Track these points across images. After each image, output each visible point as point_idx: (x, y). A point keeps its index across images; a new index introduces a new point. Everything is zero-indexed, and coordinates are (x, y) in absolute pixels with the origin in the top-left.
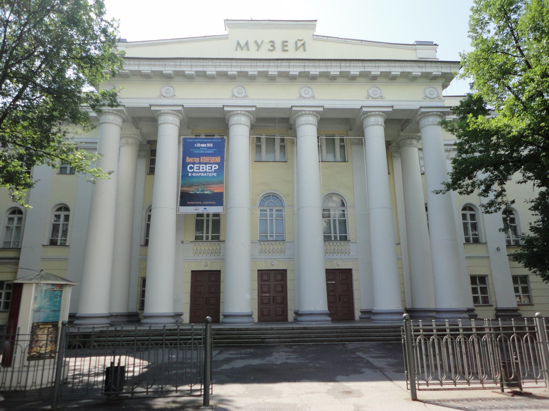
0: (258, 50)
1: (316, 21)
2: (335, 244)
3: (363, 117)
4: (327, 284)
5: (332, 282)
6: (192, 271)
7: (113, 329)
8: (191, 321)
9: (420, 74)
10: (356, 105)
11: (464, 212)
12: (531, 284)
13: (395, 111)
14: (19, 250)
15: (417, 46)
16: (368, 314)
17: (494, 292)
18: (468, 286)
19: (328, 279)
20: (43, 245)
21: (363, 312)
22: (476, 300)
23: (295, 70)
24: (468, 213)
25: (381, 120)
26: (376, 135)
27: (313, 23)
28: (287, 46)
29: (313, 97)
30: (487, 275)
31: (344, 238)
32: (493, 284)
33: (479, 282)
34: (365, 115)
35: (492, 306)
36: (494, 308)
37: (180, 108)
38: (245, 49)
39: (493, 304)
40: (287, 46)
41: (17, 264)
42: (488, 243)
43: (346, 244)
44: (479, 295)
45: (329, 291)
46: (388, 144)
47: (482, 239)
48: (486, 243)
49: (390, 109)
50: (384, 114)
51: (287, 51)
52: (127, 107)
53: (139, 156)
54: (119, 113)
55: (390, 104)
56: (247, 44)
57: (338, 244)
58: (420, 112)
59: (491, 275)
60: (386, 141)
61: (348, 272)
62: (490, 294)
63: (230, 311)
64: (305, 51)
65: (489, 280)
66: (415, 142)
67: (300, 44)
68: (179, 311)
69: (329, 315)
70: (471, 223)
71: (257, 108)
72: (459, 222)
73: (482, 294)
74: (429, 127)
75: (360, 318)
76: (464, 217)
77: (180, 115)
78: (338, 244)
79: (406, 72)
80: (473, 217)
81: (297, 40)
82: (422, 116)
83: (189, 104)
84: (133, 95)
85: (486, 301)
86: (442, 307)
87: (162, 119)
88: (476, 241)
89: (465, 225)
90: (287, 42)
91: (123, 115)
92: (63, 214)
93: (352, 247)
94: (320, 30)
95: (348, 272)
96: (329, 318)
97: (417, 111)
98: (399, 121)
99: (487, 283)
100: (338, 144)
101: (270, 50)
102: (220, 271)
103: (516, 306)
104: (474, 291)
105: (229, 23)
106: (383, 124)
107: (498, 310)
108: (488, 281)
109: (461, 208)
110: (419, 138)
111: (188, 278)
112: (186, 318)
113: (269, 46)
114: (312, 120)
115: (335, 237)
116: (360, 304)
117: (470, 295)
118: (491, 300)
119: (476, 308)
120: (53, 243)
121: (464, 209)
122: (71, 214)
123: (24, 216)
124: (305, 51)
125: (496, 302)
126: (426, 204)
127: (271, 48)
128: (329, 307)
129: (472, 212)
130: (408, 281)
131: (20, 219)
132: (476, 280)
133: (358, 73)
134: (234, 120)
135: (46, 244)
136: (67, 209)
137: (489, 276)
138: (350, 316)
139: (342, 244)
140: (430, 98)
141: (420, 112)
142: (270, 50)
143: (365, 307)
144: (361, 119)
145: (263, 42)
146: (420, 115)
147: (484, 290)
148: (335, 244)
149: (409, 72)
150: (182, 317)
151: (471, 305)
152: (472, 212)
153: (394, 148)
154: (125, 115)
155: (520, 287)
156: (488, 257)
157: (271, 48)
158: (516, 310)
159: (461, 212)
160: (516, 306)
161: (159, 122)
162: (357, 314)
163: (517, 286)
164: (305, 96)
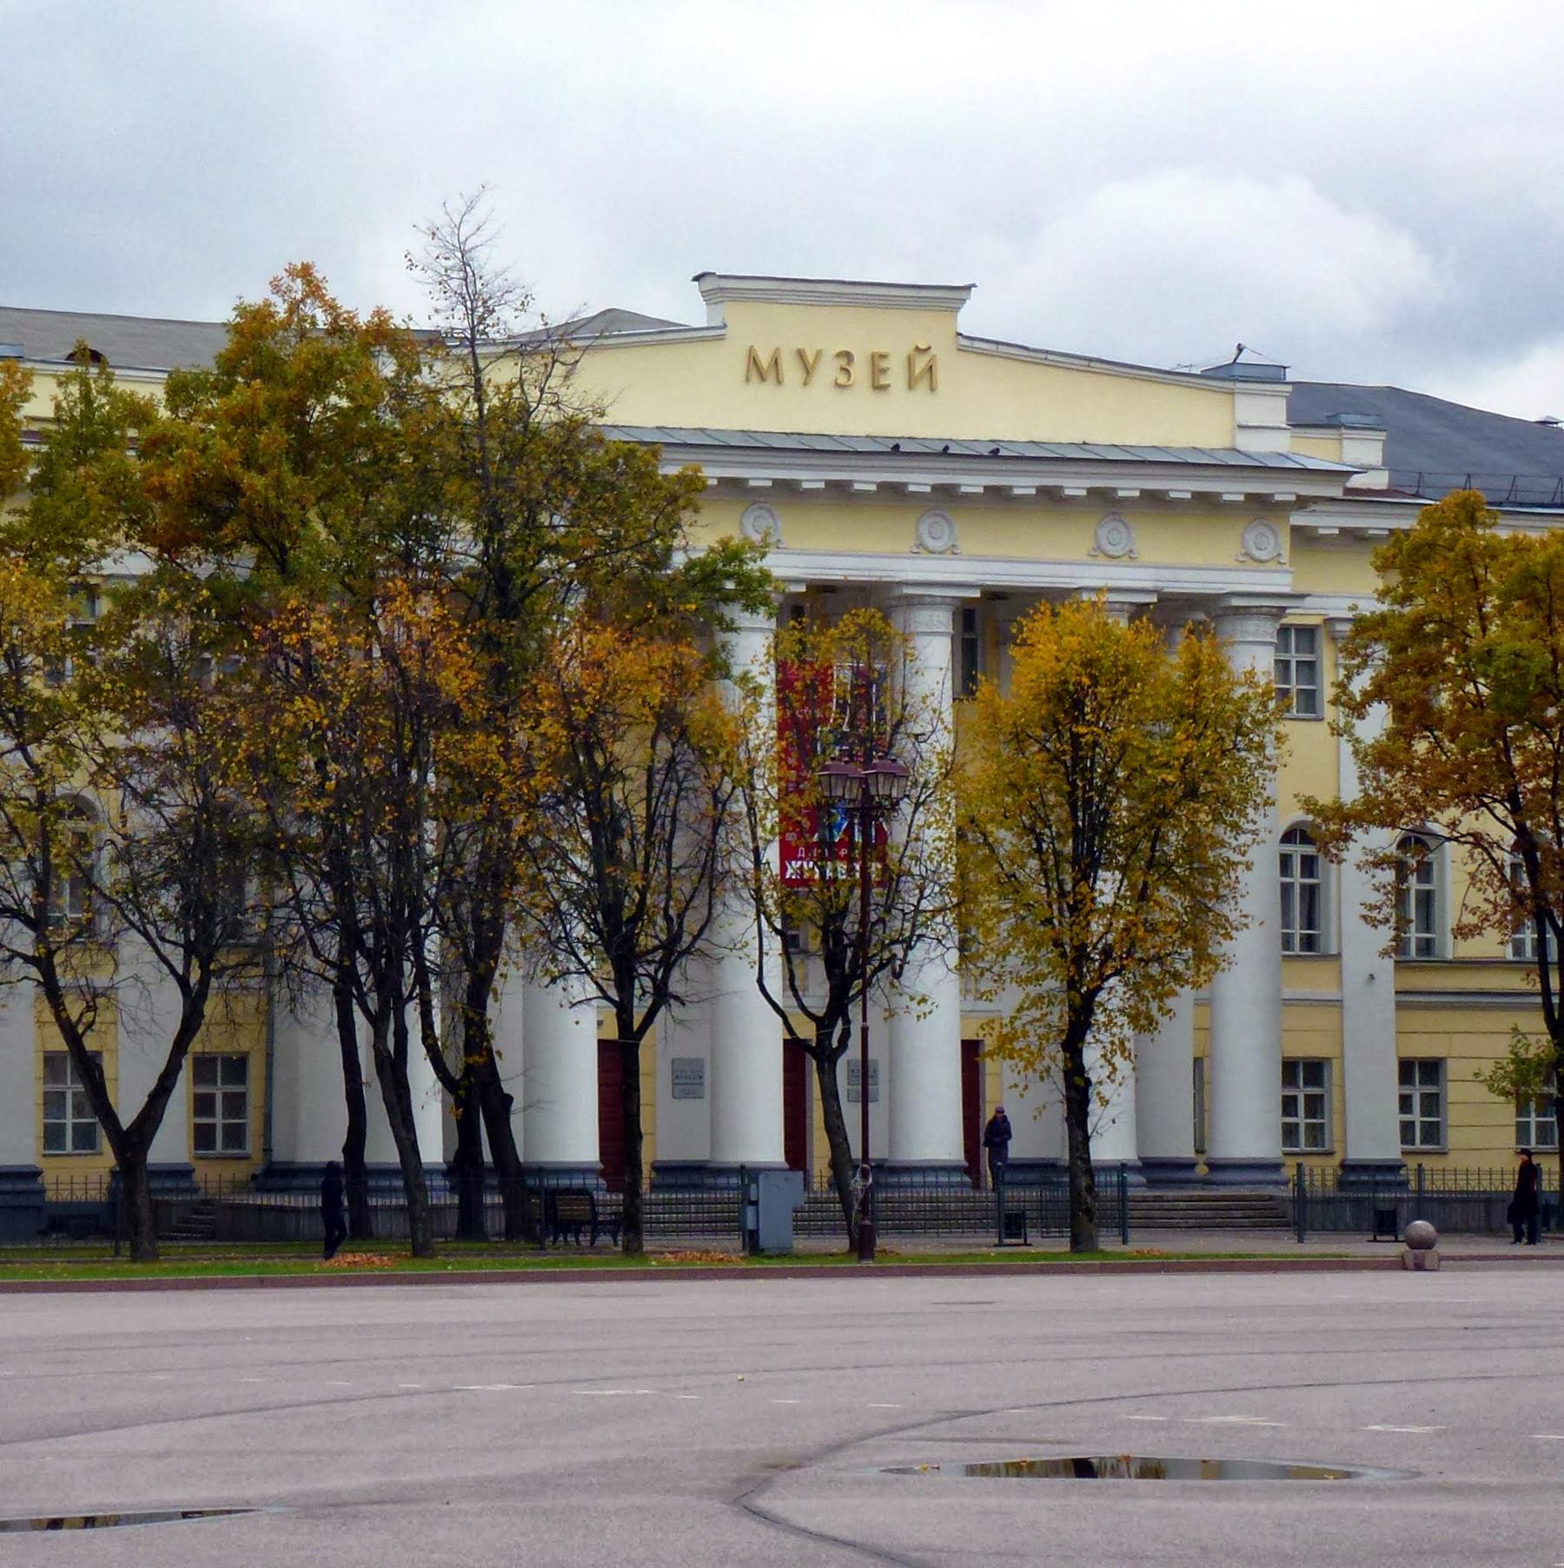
0: (805, 384)
7: (145, 1214)
11: (1288, 848)
17: (1344, 1112)
22: (1289, 1133)
24: (1298, 850)
28: (884, 371)
29: (953, 551)
30: (1328, 1059)
32: (1343, 1086)
35: (1330, 1154)
36: (1336, 1160)
38: (771, 378)
39: (1337, 1147)
40: (884, 371)
41: (1342, 1007)
42: (1345, 956)
44: (1301, 1119)
48: (1339, 955)
51: (884, 388)
56: (776, 362)
59: (1342, 1057)
62: (1331, 1120)
63: (544, 1159)
64: (932, 389)
65: (1333, 1074)
67: (921, 364)
74: (1245, 647)
81: (910, 349)
84: (799, 555)
86: (1161, 1155)
88: (1309, 943)
89: (1286, 889)
90: (883, 356)
94: (971, 319)
99: (1326, 1084)
103: (1399, 1156)
104: (1289, 1105)
107: (1347, 1167)
108: (1330, 1075)
114: (942, 620)
117: (1276, 1119)
121: (1288, 837)
124: (932, 389)
125: (1344, 1140)
127: (842, 379)
128: (601, 1154)
132: (1295, 1074)
137: (1335, 1064)
140: (1256, 560)
145: (819, 354)
147: (1315, 1106)
150: (40, 1180)
155: (1417, 1092)
156: (1338, 1003)
157: (842, 379)
158: (1393, 1168)
160: (1399, 1156)
163: (1407, 1090)
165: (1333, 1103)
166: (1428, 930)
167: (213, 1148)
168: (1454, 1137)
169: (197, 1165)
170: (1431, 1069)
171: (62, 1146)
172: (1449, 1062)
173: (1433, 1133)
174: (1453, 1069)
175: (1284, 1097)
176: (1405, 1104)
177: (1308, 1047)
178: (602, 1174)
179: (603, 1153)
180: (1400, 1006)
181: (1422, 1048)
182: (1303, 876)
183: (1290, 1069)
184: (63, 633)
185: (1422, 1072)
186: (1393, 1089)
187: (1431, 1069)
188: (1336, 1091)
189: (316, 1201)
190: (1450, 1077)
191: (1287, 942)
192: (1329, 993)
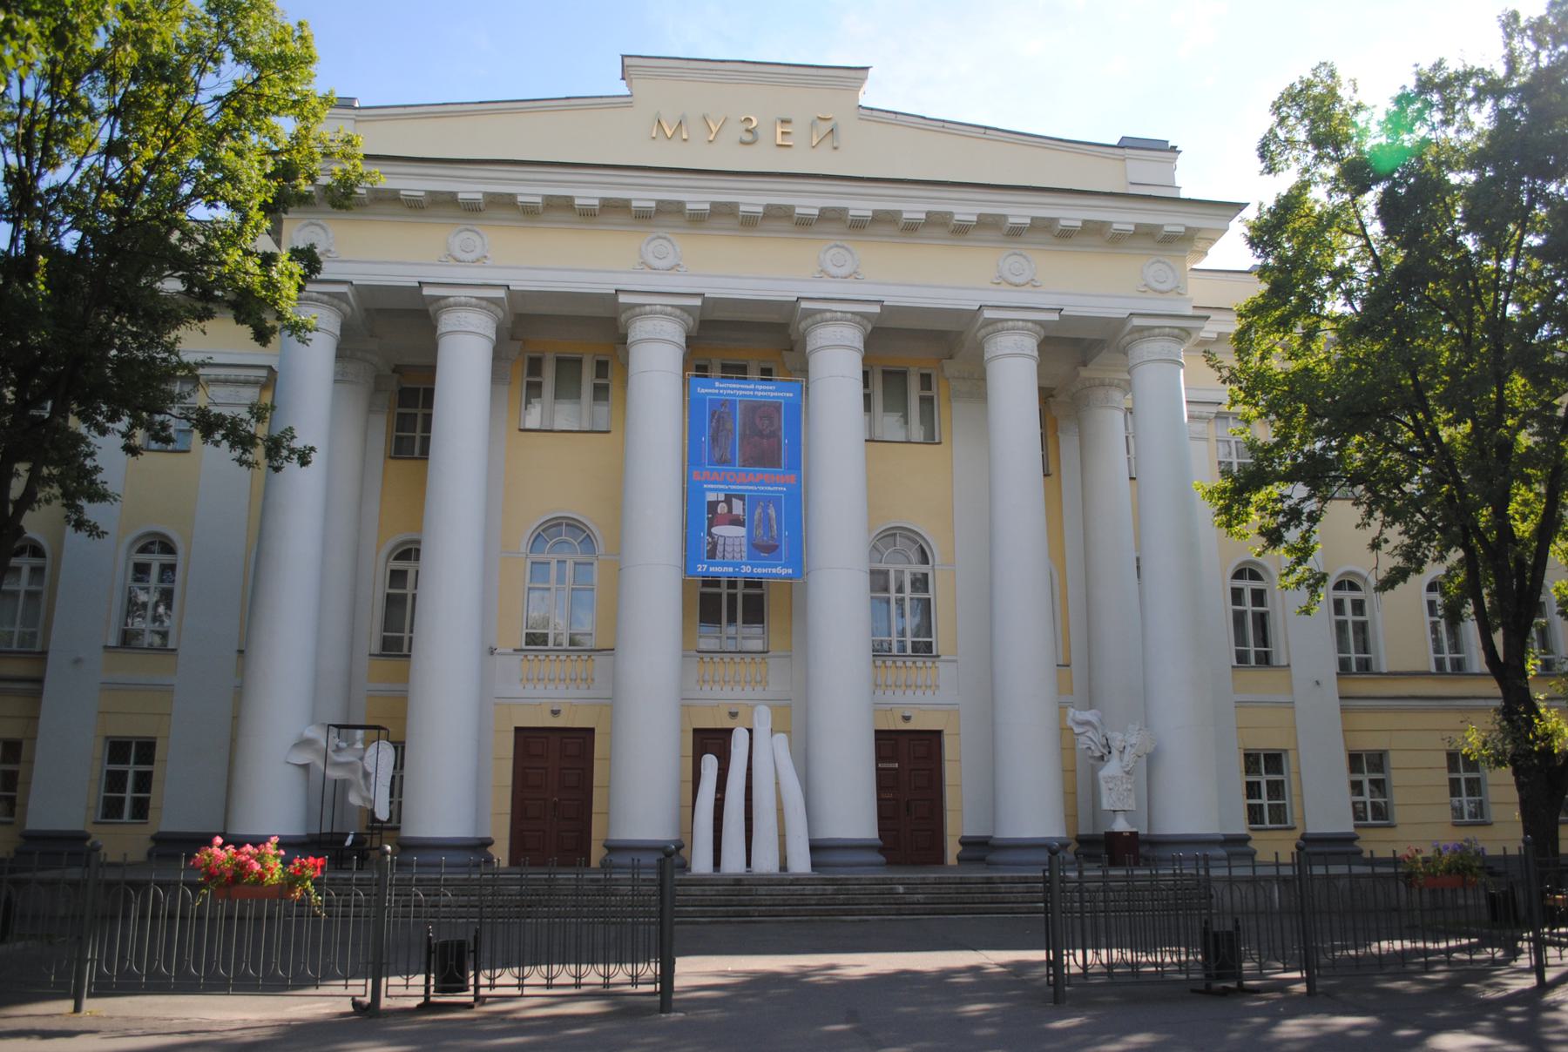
1: (867, 68)
2: (899, 664)
3: (983, 332)
4: (878, 769)
5: (891, 765)
6: (517, 729)
8: (514, 859)
9: (1132, 228)
10: (965, 300)
11: (1238, 584)
12: (1393, 772)
13: (1066, 320)
14: (43, 654)
15: (1128, 151)
16: (979, 848)
17: (1301, 795)
18: (1238, 779)
19: (880, 756)
20: (106, 647)
21: (966, 843)
22: (1254, 814)
23: (808, 202)
24: (1248, 585)
25: (1030, 344)
26: (1014, 377)
27: (860, 73)
29: (854, 276)
31: (924, 649)
33: (1265, 768)
34: (990, 328)
35: (1293, 829)
36: (1297, 834)
37: (501, 293)
41: (38, 695)
43: (929, 664)
44: (1264, 801)
45: (881, 787)
46: (1046, 395)
47: (1279, 658)
49: (1055, 317)
50: (1038, 328)
52: (357, 286)
53: (371, 409)
54: (336, 302)
55: (1052, 302)
57: (909, 664)
58: (1128, 327)
59: (1296, 749)
60: (1041, 389)
61: (933, 739)
62: (1290, 801)
65: (1289, 763)
66: (1117, 395)
68: (486, 833)
69: (881, 850)
70: (1254, 614)
71: (706, 300)
72: (1223, 609)
73: (1261, 806)
75: (960, 859)
76: (1237, 595)
77: (499, 311)
78: (909, 664)
79: (1096, 222)
80: (1259, 597)
82: (1136, 336)
83: (524, 281)
84: (368, 255)
85: (1278, 814)
87: (447, 322)
88: (1264, 660)
91: (344, 306)
92: (156, 560)
93: (944, 671)
94: (869, 97)
95: (933, 739)
96: (881, 859)
97: (1122, 322)
98: (1076, 342)
100: (914, 392)
101: (743, 143)
102: (592, 730)
104: (1252, 790)
105: (630, 66)
106: (1036, 354)
109: (1230, 571)
110: (1128, 387)
111: (506, 747)
112: (501, 853)
113: (739, 132)
114: (853, 336)
115: (903, 648)
116: (962, 819)
118: (1292, 816)
119: (1254, 835)
120: (128, 639)
122: (180, 560)
123: (48, 562)
126: (1138, 560)
129: (1257, 585)
130: (1078, 773)
131: (37, 572)
133: (975, 218)
134: (639, 330)
135: (113, 642)
136: (167, 547)
137: (1291, 754)
138: (933, 852)
139: (920, 664)
141: (1128, 327)
142: (743, 143)
143: (972, 831)
144: (980, 335)
146: (1131, 332)
147: (1276, 789)
148: (899, 664)
149: (1104, 222)
150: (489, 849)
151: (1240, 827)
152: (1257, 585)
153: (1062, 406)
154: (348, 303)
155: (1365, 778)
156: (1291, 705)
158: (1348, 839)
159: (1230, 583)
161: (442, 328)
162: (952, 850)
163: (1358, 777)
164: (834, 271)
165: (1291, 788)
166: (1365, 651)
167: (1262, 822)
168: (1398, 815)
169: (1251, 834)
170: (1378, 760)
171: (120, 816)
172: (1391, 754)
173: (1381, 812)
174: (1394, 760)
175: (1248, 783)
176: (1356, 787)
177: (1266, 742)
178: (881, 850)
179: (882, 829)
180: (1344, 710)
181: (1368, 743)
182: (1254, 605)
183: (1251, 761)
184: (1460, 309)
185: (1367, 766)
186: (1344, 777)
187: (1378, 760)
188: (1294, 777)
189: (1086, 873)
190: (1393, 765)
191: (1242, 658)
192: (1283, 698)
